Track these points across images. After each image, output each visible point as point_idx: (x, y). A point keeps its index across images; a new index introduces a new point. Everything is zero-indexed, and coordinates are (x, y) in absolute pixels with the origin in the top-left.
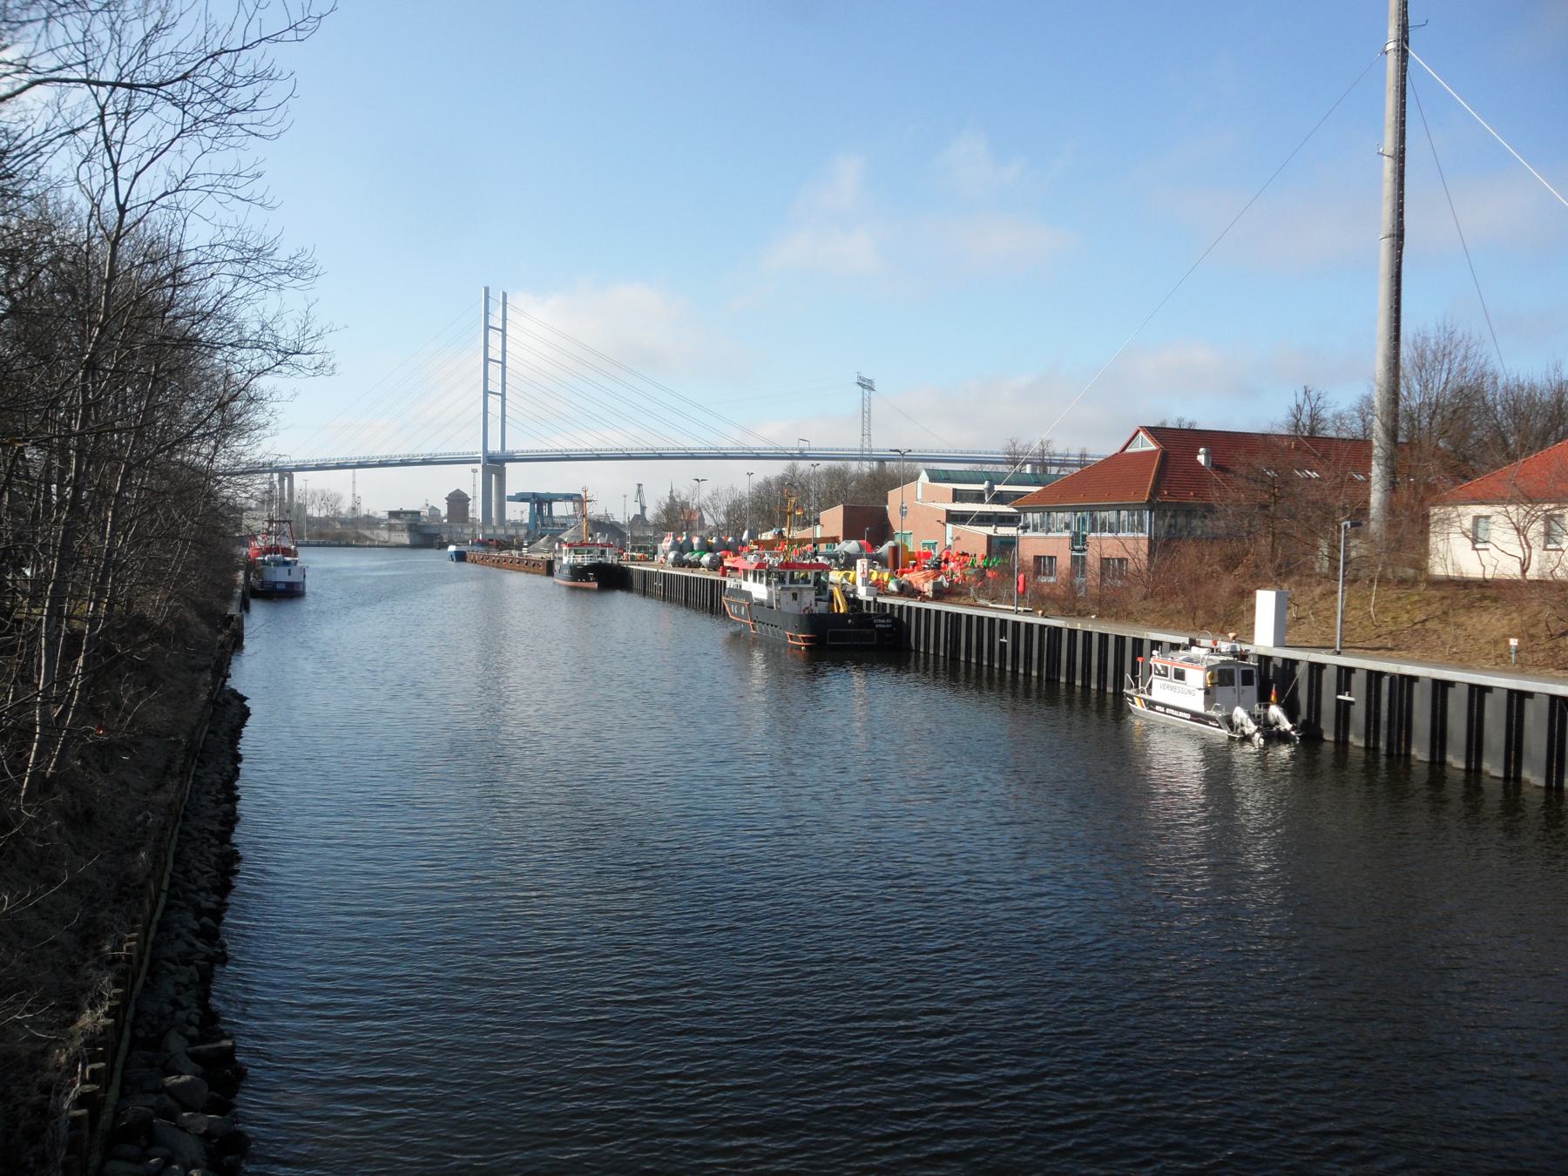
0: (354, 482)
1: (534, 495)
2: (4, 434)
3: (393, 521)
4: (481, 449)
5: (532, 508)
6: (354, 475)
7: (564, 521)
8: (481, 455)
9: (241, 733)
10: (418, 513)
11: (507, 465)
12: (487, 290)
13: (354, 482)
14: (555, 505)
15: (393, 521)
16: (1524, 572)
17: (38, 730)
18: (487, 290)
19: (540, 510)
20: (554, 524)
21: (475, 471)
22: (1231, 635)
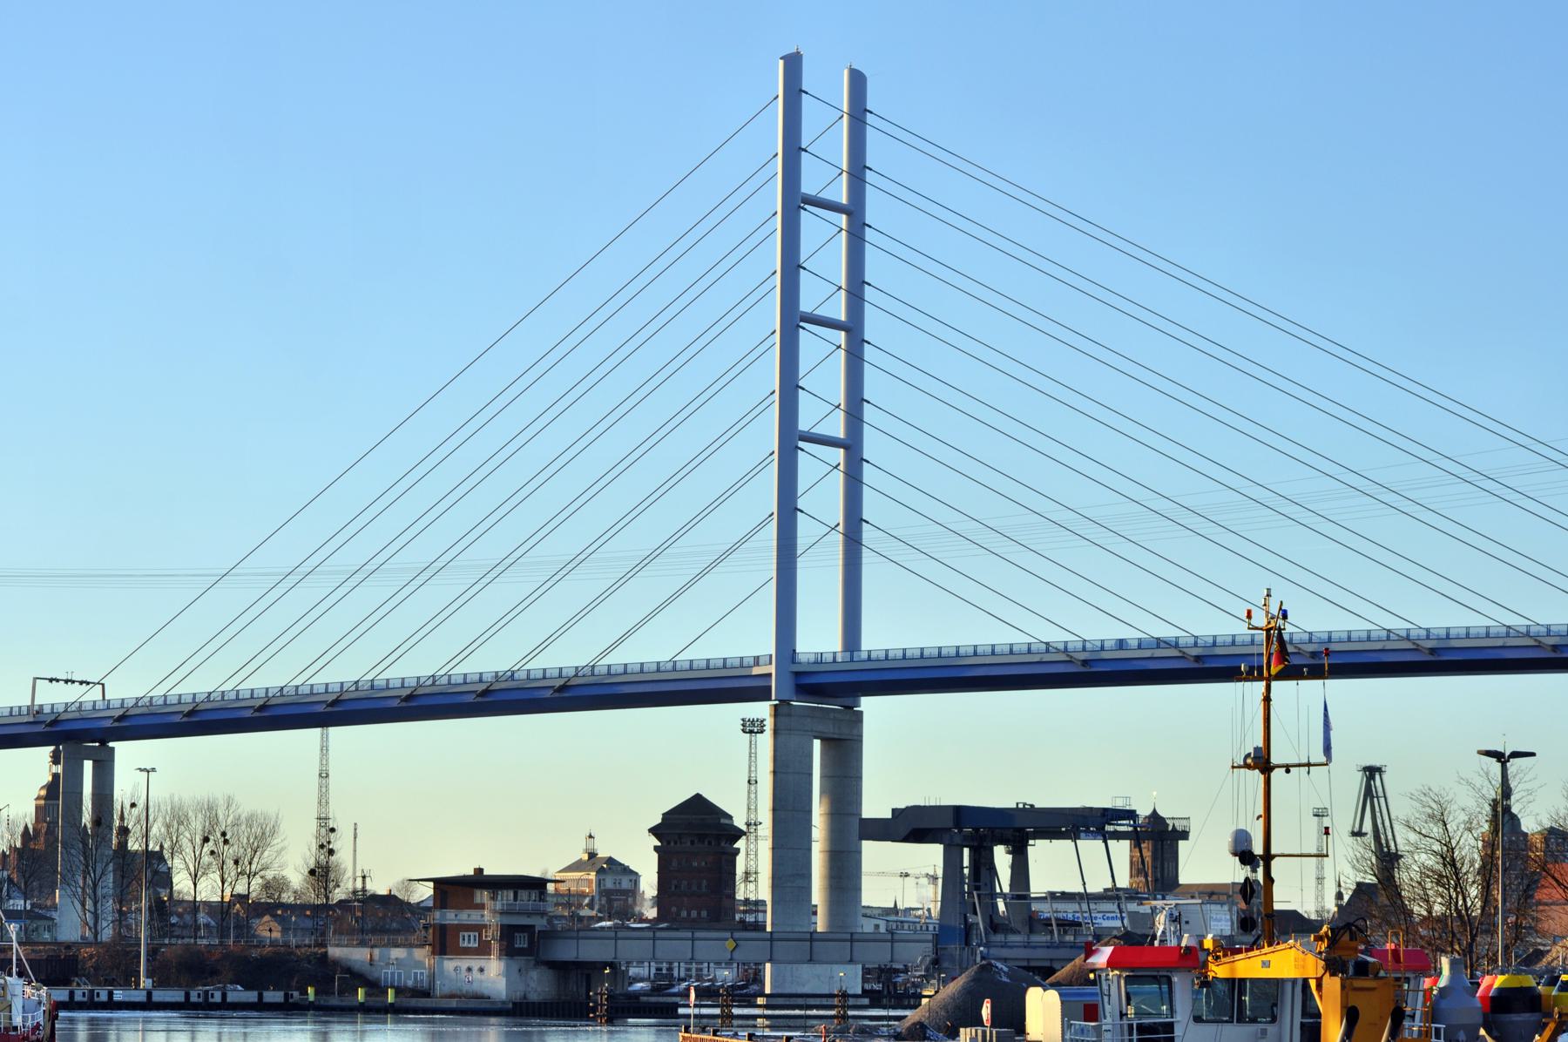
3: (451, 917)
11: (869, 705)
15: (451, 917)
20: (1034, 923)
21: (752, 728)
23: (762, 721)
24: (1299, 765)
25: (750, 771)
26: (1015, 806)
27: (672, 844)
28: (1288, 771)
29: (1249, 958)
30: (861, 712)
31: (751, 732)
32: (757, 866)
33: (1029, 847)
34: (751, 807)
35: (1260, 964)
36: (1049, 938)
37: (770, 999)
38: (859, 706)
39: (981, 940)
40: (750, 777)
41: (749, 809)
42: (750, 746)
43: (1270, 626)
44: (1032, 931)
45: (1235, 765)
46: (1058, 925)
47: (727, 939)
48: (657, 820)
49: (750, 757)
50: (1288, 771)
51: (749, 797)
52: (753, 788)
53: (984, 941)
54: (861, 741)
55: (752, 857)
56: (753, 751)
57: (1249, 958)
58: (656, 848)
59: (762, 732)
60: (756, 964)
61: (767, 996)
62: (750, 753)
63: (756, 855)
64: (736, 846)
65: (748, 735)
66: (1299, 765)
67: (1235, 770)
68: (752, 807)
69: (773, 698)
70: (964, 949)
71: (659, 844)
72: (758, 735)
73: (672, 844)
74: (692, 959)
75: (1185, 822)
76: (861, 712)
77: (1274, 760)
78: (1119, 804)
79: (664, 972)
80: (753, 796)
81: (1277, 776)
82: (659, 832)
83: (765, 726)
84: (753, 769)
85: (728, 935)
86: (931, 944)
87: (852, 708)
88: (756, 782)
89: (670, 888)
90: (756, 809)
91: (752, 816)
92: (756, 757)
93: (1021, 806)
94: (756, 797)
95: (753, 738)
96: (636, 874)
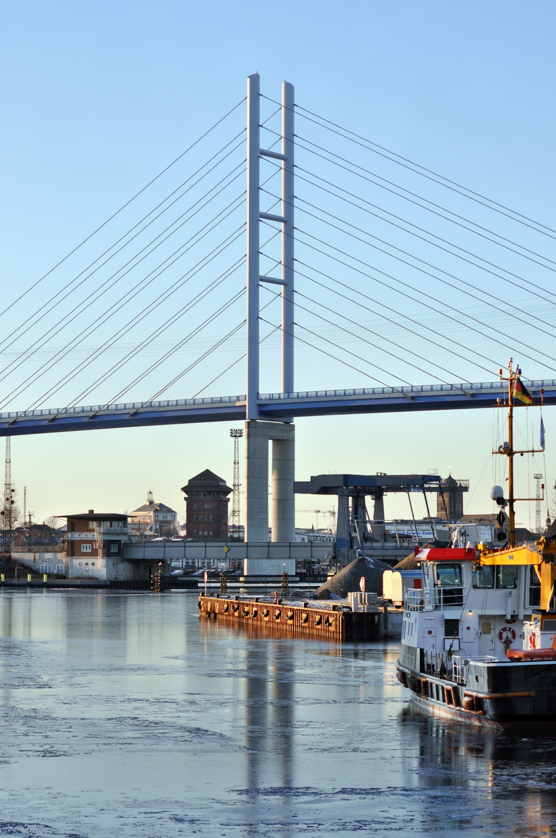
0: (8, 461)
1: (347, 478)
2: (520, 830)
4: (243, 390)
5: (342, 505)
6: (8, 448)
7: (405, 530)
8: (246, 403)
9: (189, 483)
10: (122, 518)
11: (297, 421)
12: (255, 80)
13: (8, 461)
14: (389, 498)
16: (534, 646)
17: (350, 517)
18: (255, 80)
19: (359, 506)
20: (386, 536)
21: (236, 434)
22: (510, 676)
23: (241, 431)
24: (528, 452)
25: (235, 457)
26: (376, 474)
27: (194, 496)
28: (522, 455)
29: (502, 554)
30: (294, 425)
31: (235, 436)
32: (239, 508)
33: (384, 496)
34: (236, 476)
35: (508, 557)
36: (394, 544)
37: (246, 578)
38: (293, 422)
39: (359, 545)
40: (235, 460)
41: (234, 477)
42: (235, 444)
43: (512, 378)
44: (385, 541)
45: (494, 452)
46: (399, 537)
47: (224, 547)
48: (186, 484)
49: (235, 449)
50: (522, 455)
51: (234, 471)
52: (236, 466)
53: (360, 546)
54: (294, 441)
55: (237, 503)
56: (236, 446)
57: (502, 554)
58: (185, 499)
59: (241, 436)
60: (239, 560)
61: (245, 576)
62: (235, 448)
63: (239, 502)
64: (228, 497)
65: (234, 438)
66: (528, 452)
67: (494, 454)
68: (236, 476)
69: (247, 418)
70: (349, 550)
71: (187, 496)
72: (239, 438)
73: (194, 496)
74: (205, 557)
75: (466, 482)
76: (294, 425)
77: (515, 449)
78: (431, 473)
79: (190, 564)
80: (237, 470)
81: (516, 457)
82: (187, 490)
83: (242, 433)
84: (236, 456)
85: (224, 544)
86: (332, 548)
87: (289, 423)
88: (238, 463)
89: (193, 519)
90: (238, 477)
91: (236, 481)
92: (238, 450)
93: (379, 474)
94: (238, 471)
95: (236, 440)
96: (175, 512)
